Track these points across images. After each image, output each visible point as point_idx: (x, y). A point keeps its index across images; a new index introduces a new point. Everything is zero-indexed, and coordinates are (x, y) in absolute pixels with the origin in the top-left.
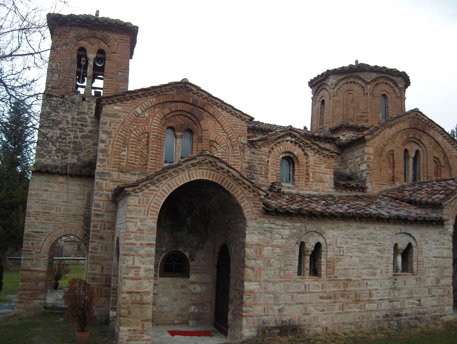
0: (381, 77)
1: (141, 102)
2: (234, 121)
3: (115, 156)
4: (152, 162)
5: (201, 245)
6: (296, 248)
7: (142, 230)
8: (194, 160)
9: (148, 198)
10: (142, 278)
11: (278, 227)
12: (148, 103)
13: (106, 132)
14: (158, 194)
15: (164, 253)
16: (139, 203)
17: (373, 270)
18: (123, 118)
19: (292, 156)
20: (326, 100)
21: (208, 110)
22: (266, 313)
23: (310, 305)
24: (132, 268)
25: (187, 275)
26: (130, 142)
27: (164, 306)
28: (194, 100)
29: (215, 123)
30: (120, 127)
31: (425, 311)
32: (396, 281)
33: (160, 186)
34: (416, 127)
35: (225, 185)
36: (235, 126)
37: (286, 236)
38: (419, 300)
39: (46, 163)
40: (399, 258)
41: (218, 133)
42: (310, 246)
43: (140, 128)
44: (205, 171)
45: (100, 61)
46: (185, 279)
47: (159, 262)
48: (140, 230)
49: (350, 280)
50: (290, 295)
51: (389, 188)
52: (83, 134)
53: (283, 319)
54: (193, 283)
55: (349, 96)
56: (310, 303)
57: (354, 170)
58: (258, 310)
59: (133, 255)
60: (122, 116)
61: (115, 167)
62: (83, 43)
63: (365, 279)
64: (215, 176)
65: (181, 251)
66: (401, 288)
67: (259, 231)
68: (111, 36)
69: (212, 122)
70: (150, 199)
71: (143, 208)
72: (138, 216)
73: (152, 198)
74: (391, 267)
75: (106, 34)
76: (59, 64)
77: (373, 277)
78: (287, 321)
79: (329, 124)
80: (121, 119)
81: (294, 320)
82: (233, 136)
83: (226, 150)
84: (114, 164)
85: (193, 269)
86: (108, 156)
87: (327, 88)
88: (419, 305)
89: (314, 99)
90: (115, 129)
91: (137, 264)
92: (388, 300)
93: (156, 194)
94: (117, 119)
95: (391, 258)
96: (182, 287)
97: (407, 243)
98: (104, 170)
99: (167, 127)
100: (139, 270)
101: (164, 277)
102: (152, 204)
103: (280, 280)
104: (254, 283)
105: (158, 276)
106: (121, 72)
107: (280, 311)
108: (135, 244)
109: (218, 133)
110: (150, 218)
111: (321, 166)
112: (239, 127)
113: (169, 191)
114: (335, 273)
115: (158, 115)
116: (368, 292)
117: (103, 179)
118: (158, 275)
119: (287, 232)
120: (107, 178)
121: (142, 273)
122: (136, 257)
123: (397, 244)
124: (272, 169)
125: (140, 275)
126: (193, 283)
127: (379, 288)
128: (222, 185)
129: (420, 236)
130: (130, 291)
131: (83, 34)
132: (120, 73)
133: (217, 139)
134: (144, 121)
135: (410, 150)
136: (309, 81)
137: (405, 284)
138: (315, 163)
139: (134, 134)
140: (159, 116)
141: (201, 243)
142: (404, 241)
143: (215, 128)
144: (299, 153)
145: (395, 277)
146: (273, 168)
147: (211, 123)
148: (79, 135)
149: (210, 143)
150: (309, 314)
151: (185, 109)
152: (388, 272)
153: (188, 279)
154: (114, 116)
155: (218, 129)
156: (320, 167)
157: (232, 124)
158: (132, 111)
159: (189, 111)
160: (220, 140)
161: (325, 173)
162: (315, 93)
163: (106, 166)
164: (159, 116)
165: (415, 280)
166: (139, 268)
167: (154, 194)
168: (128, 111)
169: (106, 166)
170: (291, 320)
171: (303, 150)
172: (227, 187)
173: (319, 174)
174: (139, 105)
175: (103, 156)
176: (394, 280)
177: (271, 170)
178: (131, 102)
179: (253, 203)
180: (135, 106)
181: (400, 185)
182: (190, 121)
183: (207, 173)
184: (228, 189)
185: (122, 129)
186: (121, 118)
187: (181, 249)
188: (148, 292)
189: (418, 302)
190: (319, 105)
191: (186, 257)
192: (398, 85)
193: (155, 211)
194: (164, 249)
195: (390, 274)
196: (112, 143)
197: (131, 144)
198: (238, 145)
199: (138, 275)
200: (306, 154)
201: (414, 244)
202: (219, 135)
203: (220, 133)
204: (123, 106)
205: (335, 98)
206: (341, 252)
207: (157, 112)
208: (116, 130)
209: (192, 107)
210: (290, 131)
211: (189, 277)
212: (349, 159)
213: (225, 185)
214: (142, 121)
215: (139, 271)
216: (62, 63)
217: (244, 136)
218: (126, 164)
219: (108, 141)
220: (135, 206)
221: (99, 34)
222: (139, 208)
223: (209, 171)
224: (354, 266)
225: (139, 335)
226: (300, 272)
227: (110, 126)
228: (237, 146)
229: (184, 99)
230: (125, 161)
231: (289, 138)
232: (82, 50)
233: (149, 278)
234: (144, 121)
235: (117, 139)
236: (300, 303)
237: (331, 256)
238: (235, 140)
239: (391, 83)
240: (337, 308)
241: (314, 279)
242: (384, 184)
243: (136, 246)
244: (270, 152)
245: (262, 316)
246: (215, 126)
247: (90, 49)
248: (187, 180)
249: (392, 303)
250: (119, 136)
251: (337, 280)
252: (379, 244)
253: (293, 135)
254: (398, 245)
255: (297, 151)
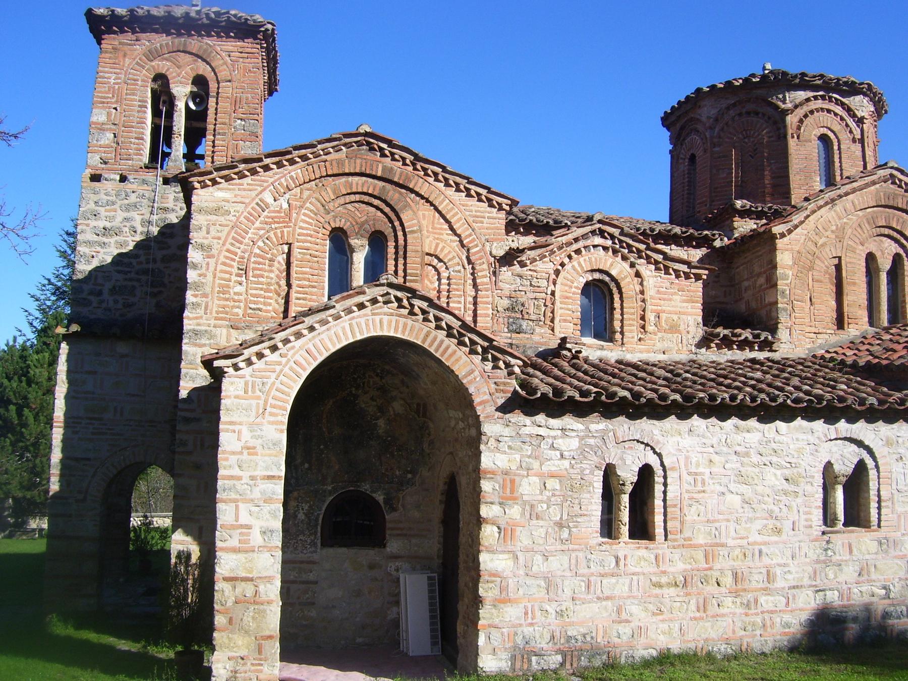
0: (816, 98)
1: (272, 180)
2: (473, 209)
3: (221, 295)
4: (300, 304)
5: (409, 476)
6: (596, 479)
7: (254, 448)
8: (362, 296)
9: (265, 380)
10: (256, 549)
11: (553, 433)
12: (286, 180)
13: (202, 247)
14: (286, 370)
15: (330, 496)
16: (246, 392)
17: (775, 521)
18: (235, 216)
19: (607, 279)
20: (699, 153)
21: (417, 189)
22: (530, 621)
23: (628, 602)
24: (233, 527)
25: (381, 543)
26: (252, 265)
27: (334, 607)
28: (384, 169)
29: (434, 216)
30: (229, 234)
31: (900, 610)
32: (831, 546)
33: (290, 353)
34: (891, 203)
35: (430, 346)
36: (478, 218)
37: (572, 453)
38: (884, 588)
39: (92, 317)
40: (839, 495)
41: (441, 237)
42: (629, 475)
43: (272, 234)
44: (386, 318)
45: (198, 100)
46: (377, 549)
47: (318, 515)
48: (248, 448)
49: (723, 545)
50: (583, 581)
51: (834, 339)
52: (165, 252)
53: (569, 633)
54: (395, 557)
55: (746, 143)
56: (629, 597)
57: (753, 305)
58: (512, 613)
59: (235, 501)
60: (232, 211)
61: (222, 318)
62: (162, 66)
63: (755, 543)
64: (408, 328)
65: (366, 490)
66: (842, 561)
67: (510, 444)
68: (219, 45)
69: (303, 211)
70: (270, 381)
71: (254, 402)
72: (245, 419)
73: (273, 379)
74: (817, 515)
75: (207, 44)
76: (114, 111)
77: (774, 538)
78: (579, 637)
79: (706, 205)
80: (231, 217)
81: (594, 635)
82: (473, 240)
83: (459, 272)
84: (217, 312)
85: (392, 529)
86: (205, 295)
87: (699, 127)
88: (884, 598)
89: (674, 155)
90: (219, 238)
91: (244, 519)
92: (811, 589)
93: (281, 371)
94: (222, 219)
95: (817, 496)
96: (372, 567)
97: (855, 461)
98: (199, 325)
99: (330, 229)
100: (250, 533)
101: (332, 546)
102: (274, 392)
103: (559, 547)
104: (501, 556)
105: (319, 544)
106: (241, 119)
107: (562, 616)
108: (239, 478)
109: (441, 237)
110: (272, 423)
111: (675, 297)
112: (485, 220)
113: (309, 364)
114: (685, 531)
115: (308, 205)
116: (764, 571)
117: (196, 345)
118: (319, 542)
119: (571, 444)
120: (203, 341)
121: (256, 539)
122: (241, 505)
123: (832, 465)
124: (561, 308)
125: (251, 542)
126: (395, 557)
127: (790, 561)
128: (426, 346)
129: (884, 443)
130: (232, 575)
131: (161, 46)
132: (239, 121)
133: (439, 249)
134: (281, 220)
135: (878, 255)
136: (663, 115)
137: (851, 551)
138: (658, 292)
139: (259, 248)
140: (312, 208)
141: (410, 472)
142: (848, 455)
143: (433, 226)
144: (621, 272)
145: (826, 537)
146: (563, 306)
147: (424, 215)
148: (159, 255)
149: (423, 259)
150: (627, 621)
151: (368, 190)
152: (811, 527)
153: (382, 550)
154: (216, 211)
155: (441, 229)
156: (670, 300)
157: (469, 215)
158: (253, 199)
159: (375, 193)
160: (446, 251)
161: (684, 314)
162: (677, 140)
163: (201, 317)
164: (312, 208)
165: (876, 543)
166: (249, 527)
167: (278, 371)
168: (247, 201)
169: (201, 317)
170: (587, 634)
171: (632, 265)
172: (437, 351)
173: (669, 315)
174: (269, 186)
175: (195, 296)
176: (825, 543)
177: (560, 312)
178: (250, 182)
179: (495, 383)
180: (260, 189)
181: (858, 333)
182: (379, 213)
183: (390, 322)
184: (437, 355)
185: (234, 238)
186: (231, 215)
187: (366, 487)
188: (270, 577)
189: (883, 592)
190: (684, 166)
191: (377, 503)
192: (856, 112)
193: (280, 408)
194: (330, 488)
195: (816, 530)
196: (213, 269)
197: (254, 269)
198: (484, 260)
199: (247, 542)
200: (638, 275)
201: (870, 463)
202: (442, 240)
203: (445, 237)
204: (234, 190)
205: (717, 149)
206: (700, 484)
207: (308, 199)
208: (221, 242)
209: (381, 184)
210: (601, 225)
211: (385, 546)
212: (744, 280)
213: (430, 346)
214: (276, 220)
215: (248, 534)
216: (118, 108)
217: (499, 239)
218: (245, 310)
219: (204, 265)
220: (237, 397)
221: (195, 43)
222: (246, 402)
223: (394, 318)
224: (731, 513)
225: (253, 668)
226: (608, 529)
227: (208, 233)
228: (484, 263)
229: (363, 169)
230: (242, 305)
231: (598, 240)
232: (161, 79)
233: (270, 549)
234: (281, 220)
235: (224, 260)
236: (607, 598)
237: (677, 494)
238: (478, 249)
239: (838, 110)
240: (693, 606)
241: (638, 545)
242: (820, 331)
243: (242, 482)
244: (557, 272)
245: (521, 625)
246: (433, 223)
247: (174, 77)
248: (347, 339)
249: (820, 593)
250: (228, 254)
251: (690, 546)
252: (788, 465)
253: (609, 234)
254: (834, 466)
255: (619, 268)
